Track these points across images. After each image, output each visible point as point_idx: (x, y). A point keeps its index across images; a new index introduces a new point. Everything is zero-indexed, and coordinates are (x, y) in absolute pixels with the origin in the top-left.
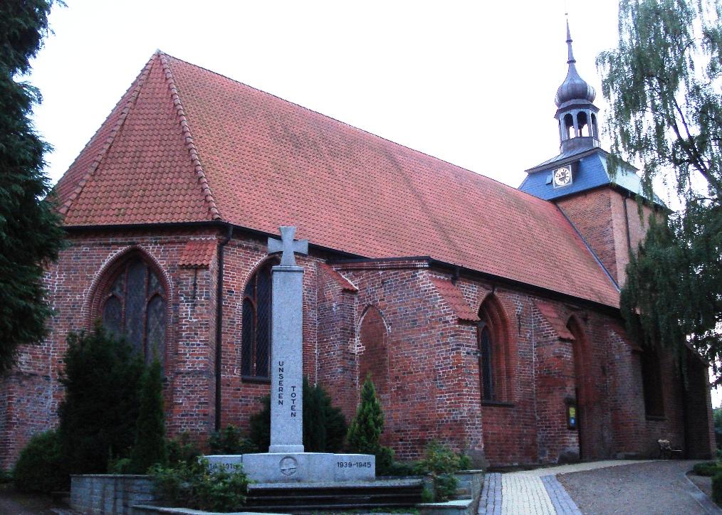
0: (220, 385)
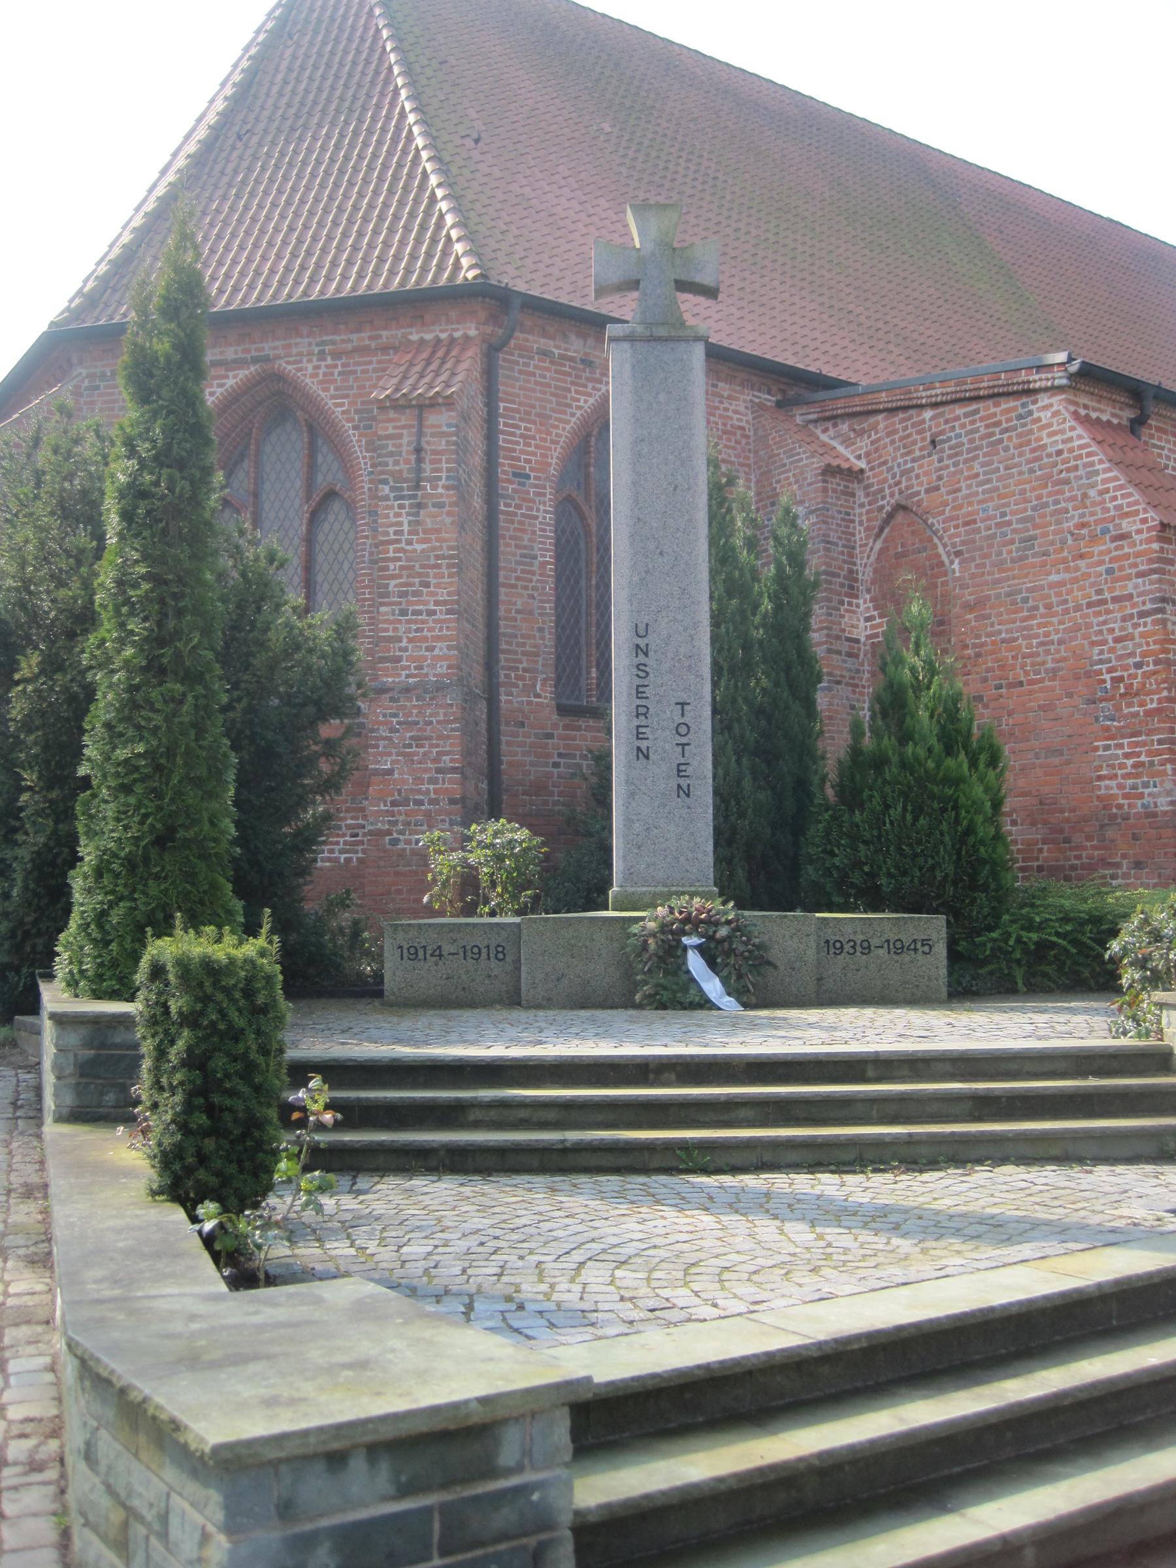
0: (498, 723)
